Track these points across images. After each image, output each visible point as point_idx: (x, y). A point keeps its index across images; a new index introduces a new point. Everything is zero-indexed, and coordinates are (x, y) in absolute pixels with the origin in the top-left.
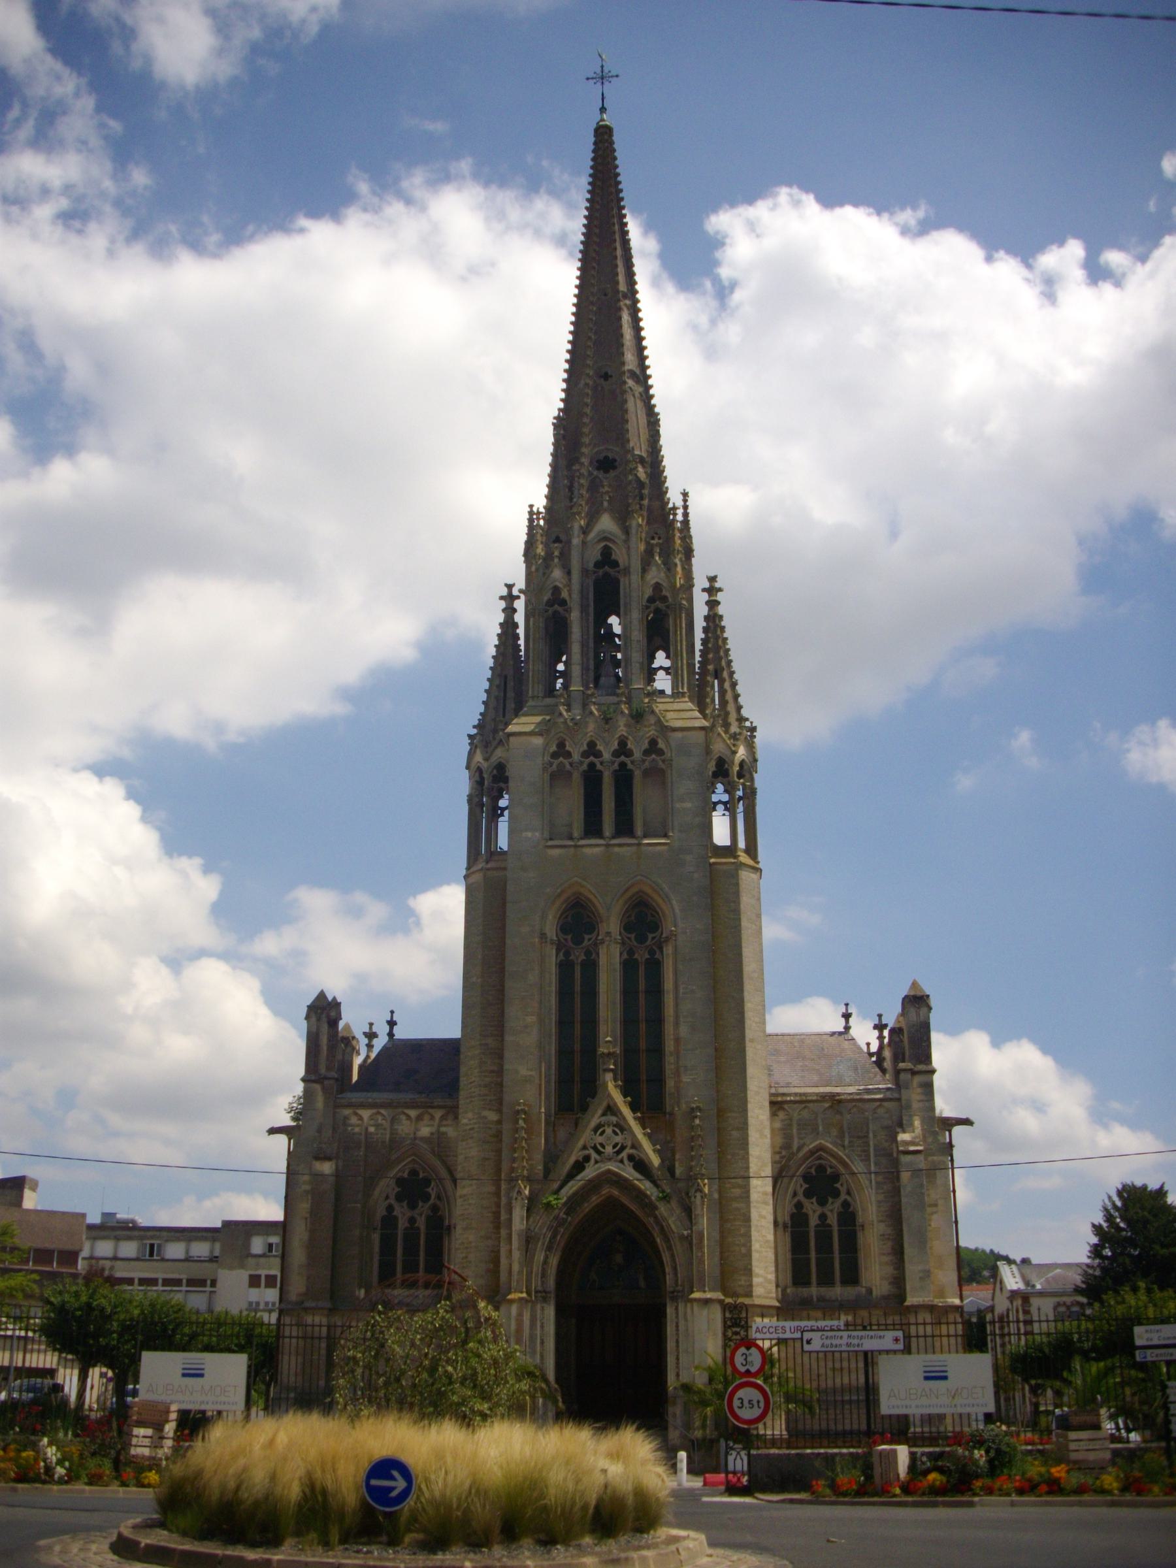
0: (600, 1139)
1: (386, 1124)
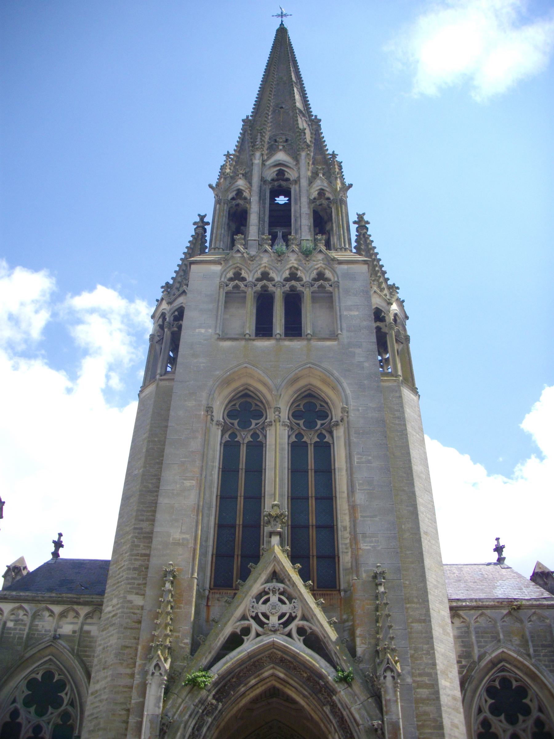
0: (263, 608)
1: (27, 620)
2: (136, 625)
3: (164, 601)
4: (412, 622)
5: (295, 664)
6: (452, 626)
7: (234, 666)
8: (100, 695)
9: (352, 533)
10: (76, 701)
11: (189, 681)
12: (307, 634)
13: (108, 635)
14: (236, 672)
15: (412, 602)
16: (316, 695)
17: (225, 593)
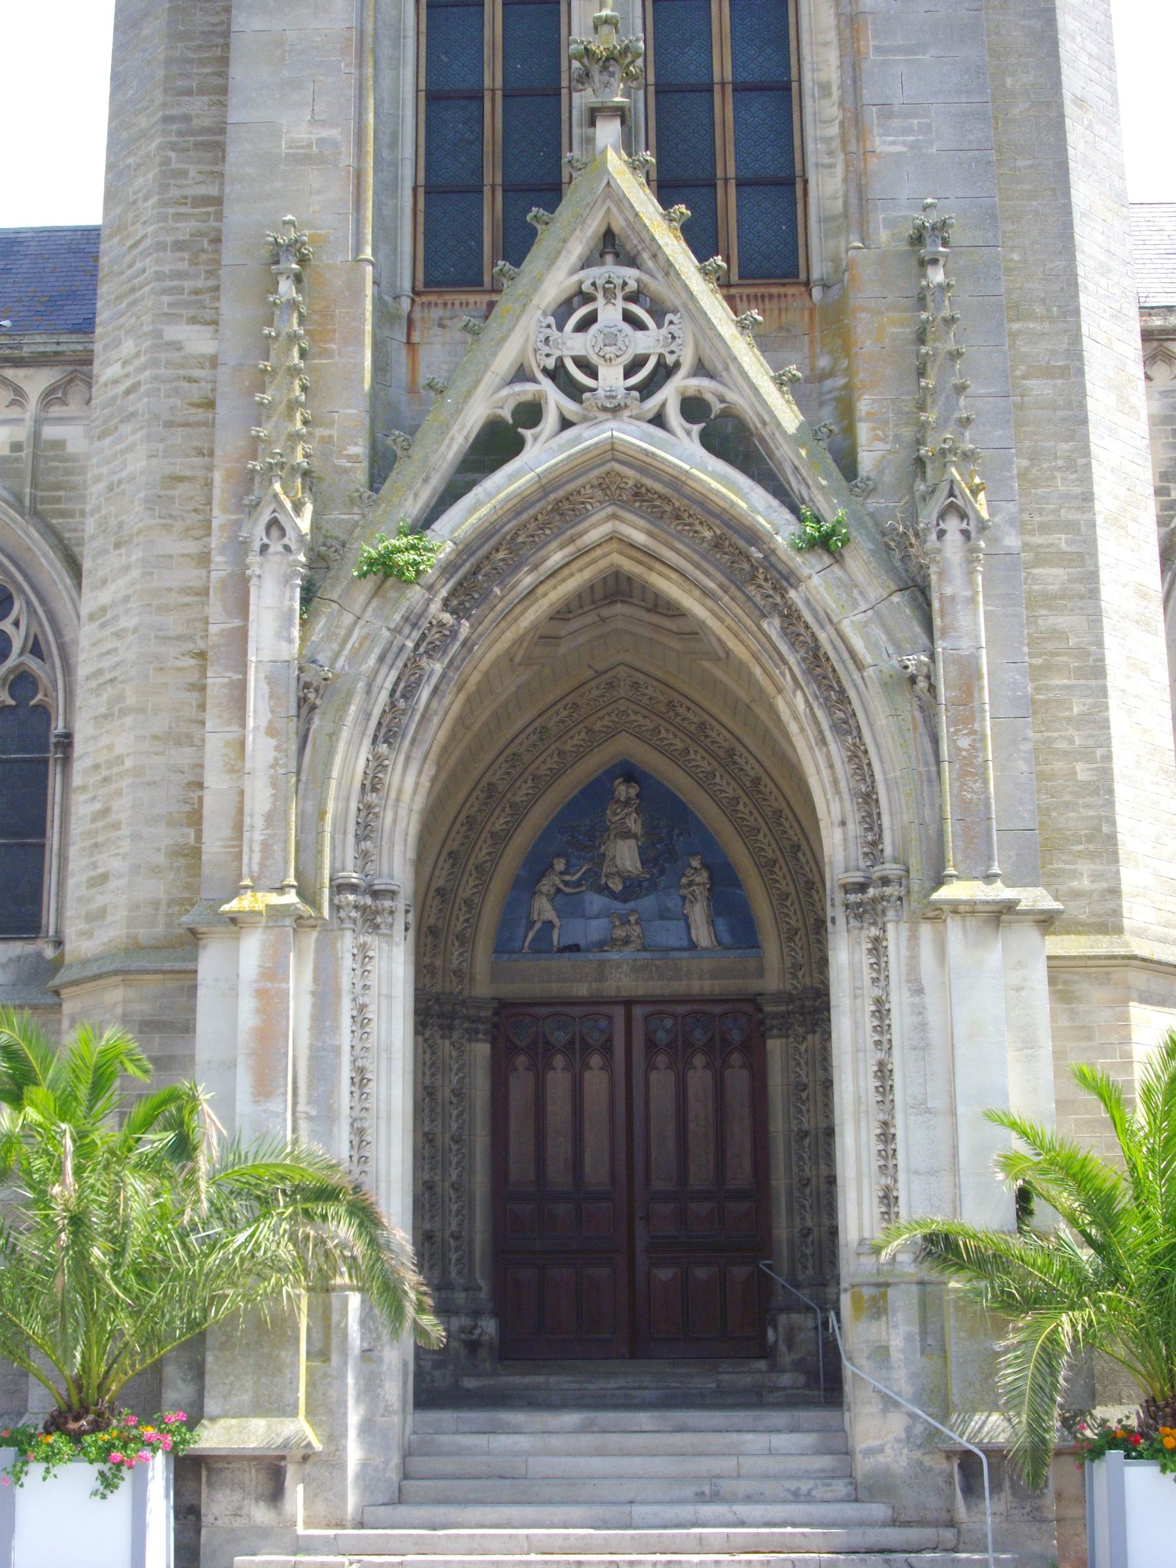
0: (575, 344)
2: (200, 414)
3: (278, 335)
4: (1024, 377)
5: (677, 504)
6: (1147, 387)
7: (500, 517)
8: (116, 618)
9: (849, 104)
10: (47, 642)
11: (371, 565)
12: (712, 416)
13: (119, 447)
14: (507, 534)
15: (1032, 317)
16: (740, 589)
17: (461, 304)
